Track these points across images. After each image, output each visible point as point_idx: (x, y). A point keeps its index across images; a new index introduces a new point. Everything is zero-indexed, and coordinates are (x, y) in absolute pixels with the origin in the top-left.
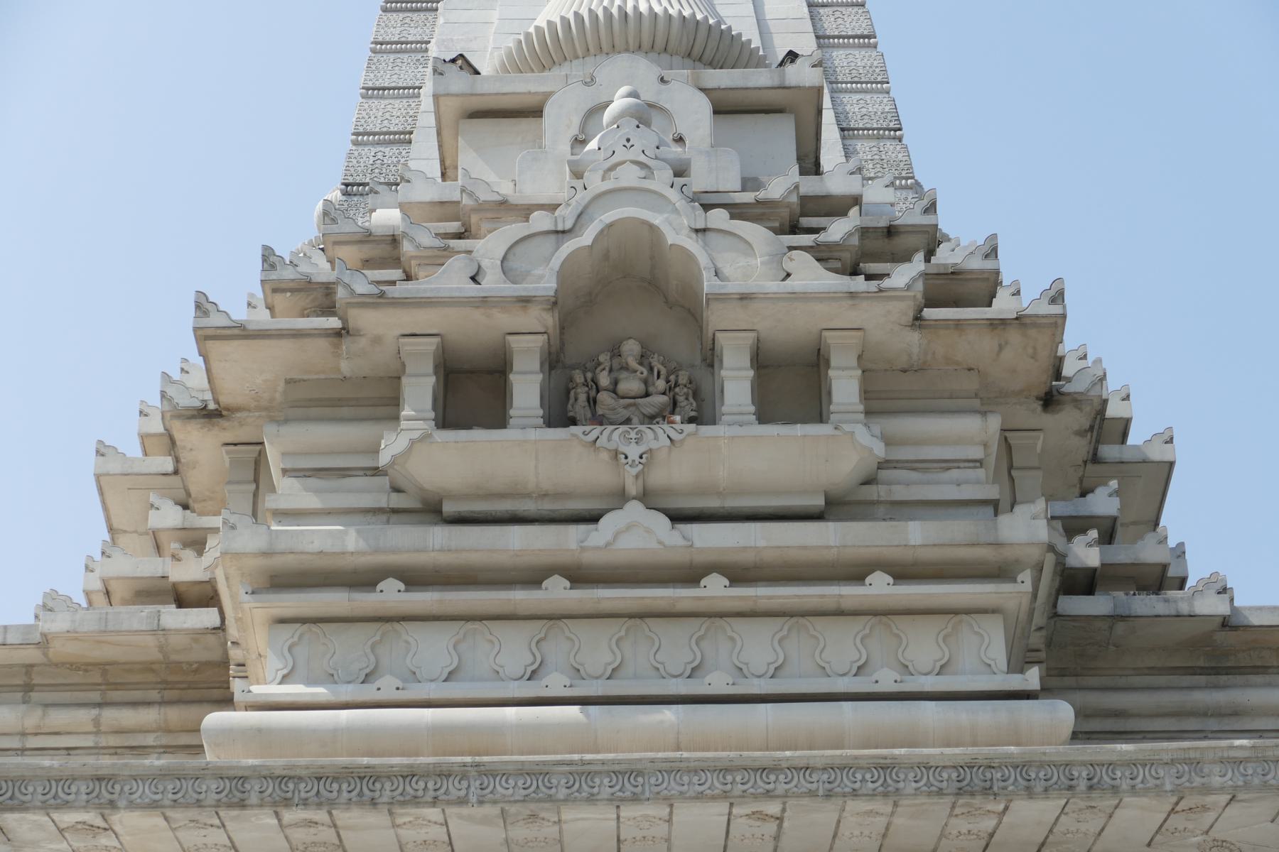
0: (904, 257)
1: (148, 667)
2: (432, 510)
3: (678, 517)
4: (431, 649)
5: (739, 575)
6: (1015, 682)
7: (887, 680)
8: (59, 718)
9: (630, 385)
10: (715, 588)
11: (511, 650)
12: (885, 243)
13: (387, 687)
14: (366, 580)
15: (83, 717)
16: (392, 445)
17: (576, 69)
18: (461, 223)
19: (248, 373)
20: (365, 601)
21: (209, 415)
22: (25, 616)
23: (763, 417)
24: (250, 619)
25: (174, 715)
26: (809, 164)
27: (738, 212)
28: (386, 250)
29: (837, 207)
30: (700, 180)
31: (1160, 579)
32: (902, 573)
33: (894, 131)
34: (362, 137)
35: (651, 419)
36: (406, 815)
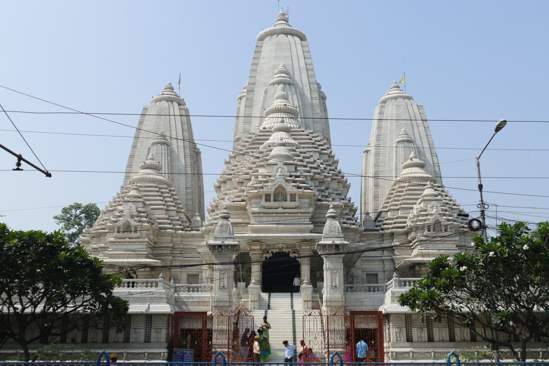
5: (288, 213)
14: (260, 213)
22: (49, 226)
26: (264, 343)
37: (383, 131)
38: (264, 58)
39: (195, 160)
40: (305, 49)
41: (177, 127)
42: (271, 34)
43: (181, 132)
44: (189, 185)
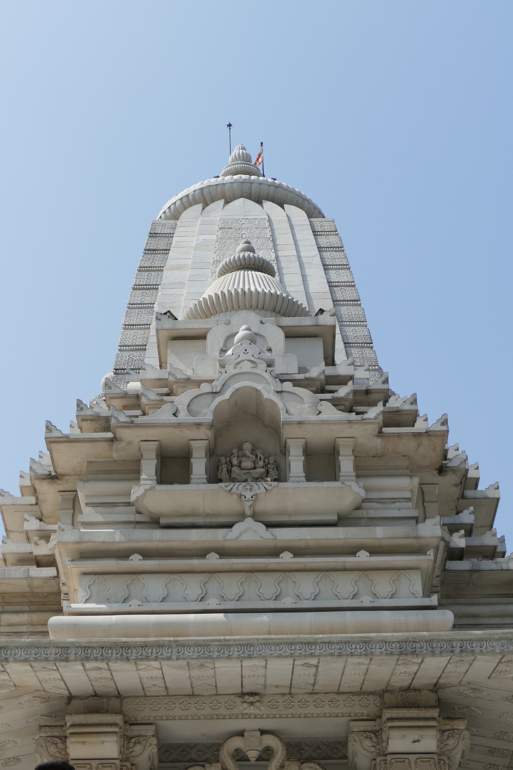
0: (374, 404)
1: (23, 595)
2: (155, 522)
3: (269, 525)
4: (155, 586)
6: (426, 602)
7: (366, 601)
9: (247, 464)
10: (287, 558)
11: (192, 587)
12: (365, 397)
13: (134, 604)
14: (124, 554)
16: (137, 492)
17: (221, 318)
18: (169, 389)
19: (71, 459)
21: (52, 478)
23: (309, 478)
24: (70, 572)
25: (36, 617)
27: (297, 383)
28: (134, 401)
29: (343, 380)
30: (279, 368)
31: (494, 553)
32: (374, 551)
33: (369, 344)
34: (123, 348)
35: (256, 479)
36: (143, 665)
38: (180, 268)
40: (323, 241)
42: (205, 198)
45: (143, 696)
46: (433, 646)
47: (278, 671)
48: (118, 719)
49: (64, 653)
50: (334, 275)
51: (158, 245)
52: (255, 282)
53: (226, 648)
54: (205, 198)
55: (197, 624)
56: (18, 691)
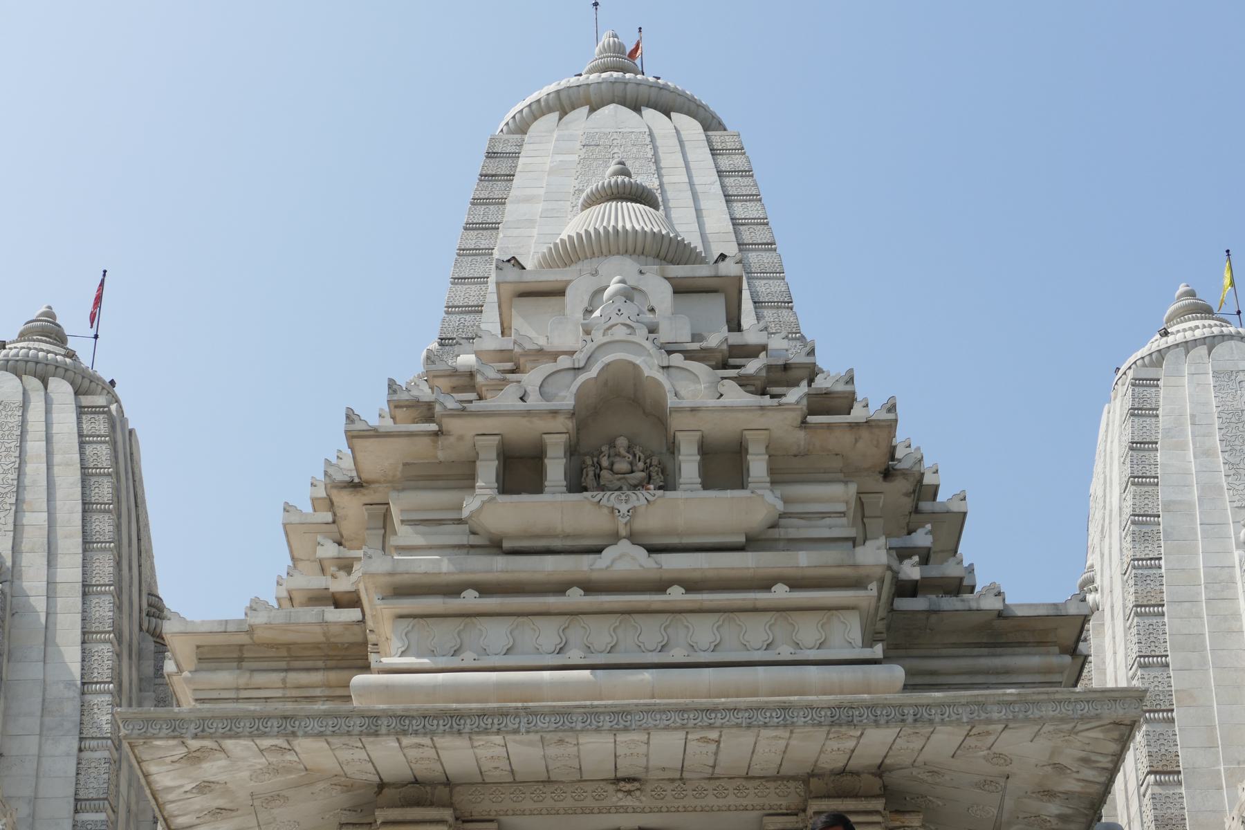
0: (795, 384)
1: (317, 646)
2: (496, 546)
3: (652, 550)
4: (496, 634)
5: (692, 586)
6: (867, 653)
7: (785, 653)
8: (260, 679)
9: (622, 466)
10: (676, 595)
11: (547, 634)
12: (782, 375)
13: (468, 658)
14: (453, 590)
15: (275, 677)
16: (470, 505)
17: (586, 266)
19: (380, 460)
20: (453, 604)
21: (355, 486)
23: (706, 486)
24: (381, 616)
25: (333, 676)
27: (689, 355)
28: (466, 381)
29: (752, 352)
30: (665, 335)
31: (958, 587)
32: (795, 584)
33: (787, 304)
34: (451, 309)
35: (634, 487)
36: (480, 740)
37: (1163, 493)
38: (528, 200)
39: (149, 669)
40: (725, 163)
41: (60, 494)
42: (563, 104)
43: (78, 517)
44: (95, 785)
45: (481, 782)
46: (876, 714)
47: (665, 748)
48: (447, 814)
49: (372, 724)
50: (740, 210)
51: (498, 169)
52: (632, 217)
53: (593, 717)
54: (563, 104)
55: (552, 684)
56: (309, 777)
